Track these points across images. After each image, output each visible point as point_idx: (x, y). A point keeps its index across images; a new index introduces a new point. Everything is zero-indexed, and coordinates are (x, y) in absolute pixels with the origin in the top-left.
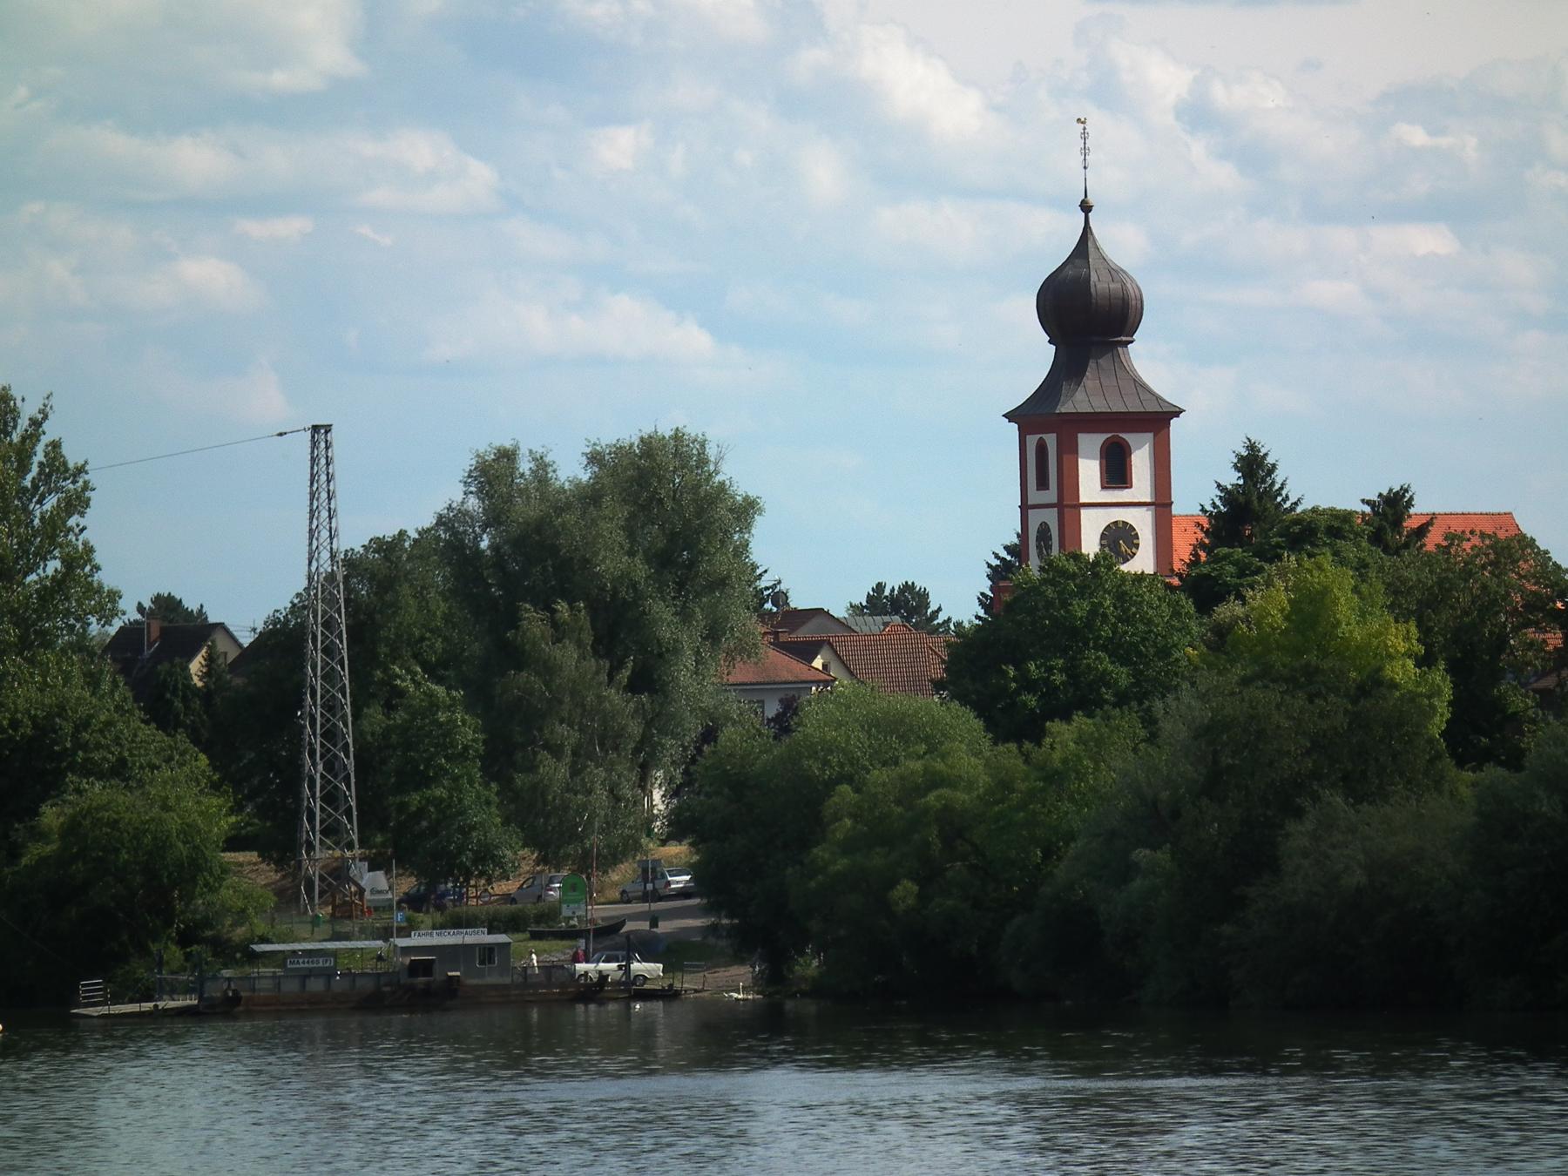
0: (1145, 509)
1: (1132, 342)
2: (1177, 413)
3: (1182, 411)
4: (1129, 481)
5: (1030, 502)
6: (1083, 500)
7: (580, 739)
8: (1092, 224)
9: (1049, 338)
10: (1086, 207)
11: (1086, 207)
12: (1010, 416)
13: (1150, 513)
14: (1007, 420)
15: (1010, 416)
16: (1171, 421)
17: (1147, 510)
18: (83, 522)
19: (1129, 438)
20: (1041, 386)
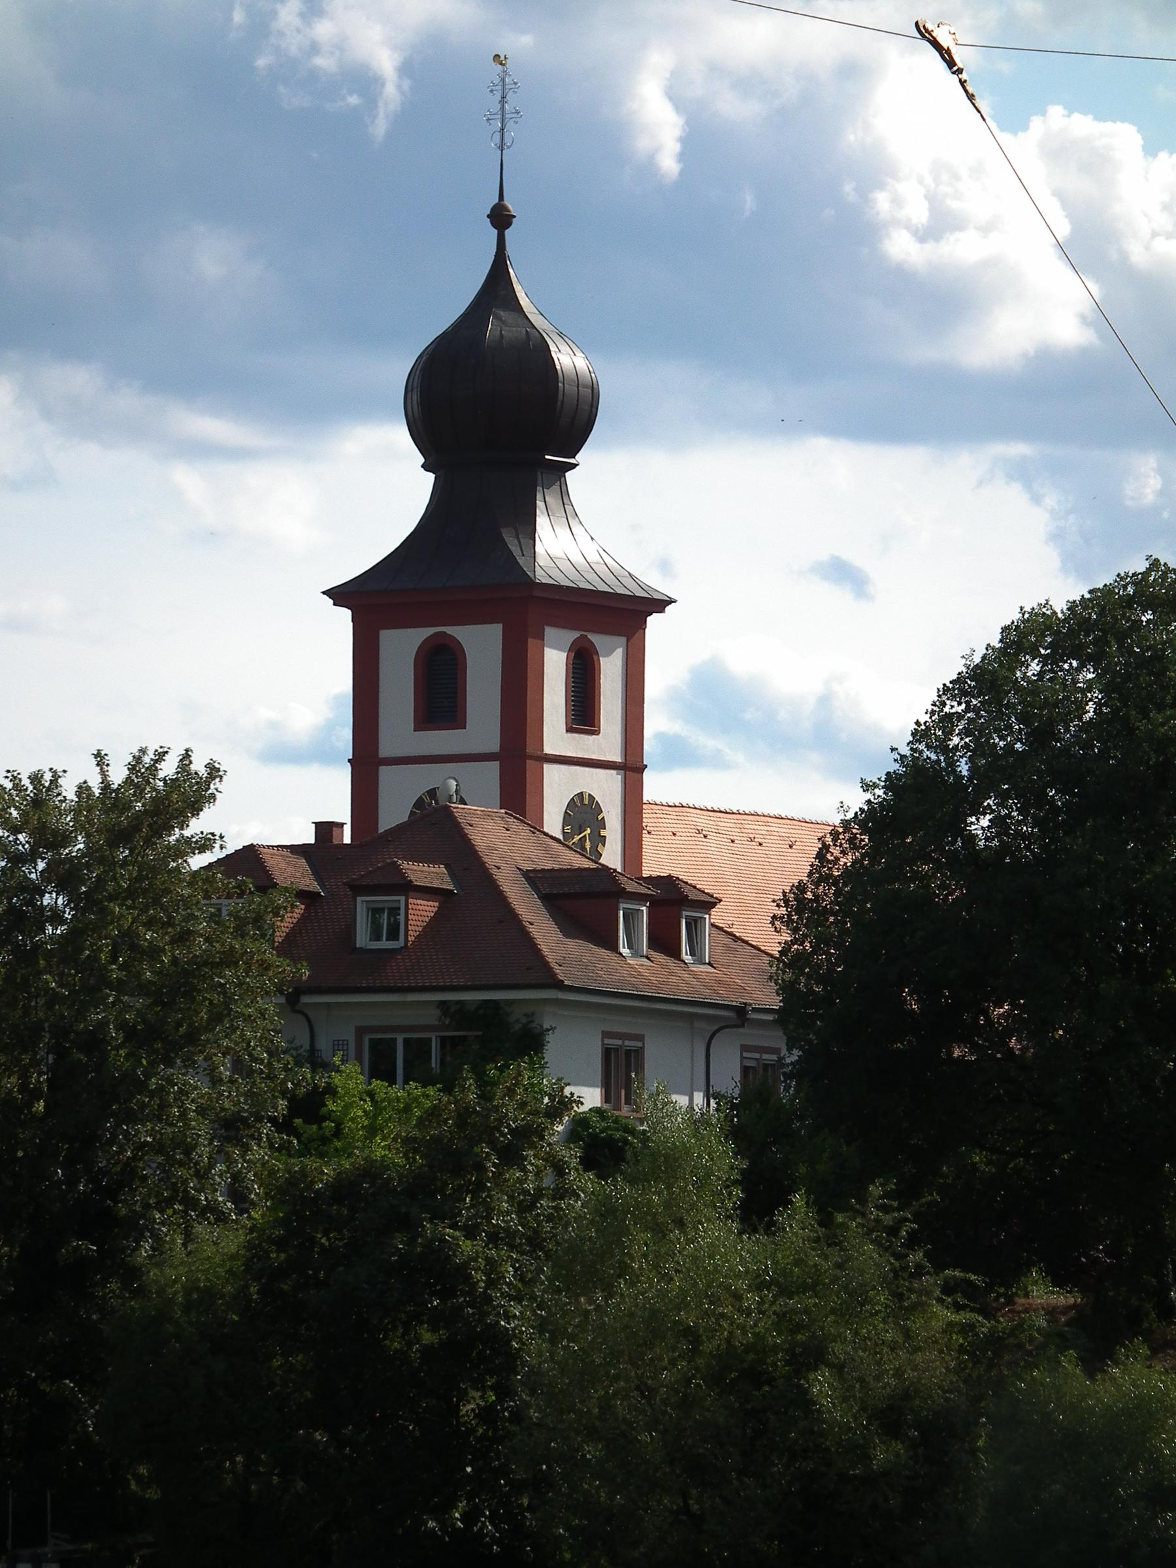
0: (614, 772)
1: (574, 466)
2: (660, 604)
3: (671, 601)
4: (596, 725)
5: (385, 751)
6: (548, 749)
7: (223, 1297)
8: (510, 250)
9: (423, 460)
10: (500, 218)
11: (500, 218)
12: (338, 595)
13: (620, 777)
14: (331, 601)
15: (338, 595)
16: (649, 619)
17: (617, 774)
18: (47, 770)
19: (597, 639)
20: (397, 549)
